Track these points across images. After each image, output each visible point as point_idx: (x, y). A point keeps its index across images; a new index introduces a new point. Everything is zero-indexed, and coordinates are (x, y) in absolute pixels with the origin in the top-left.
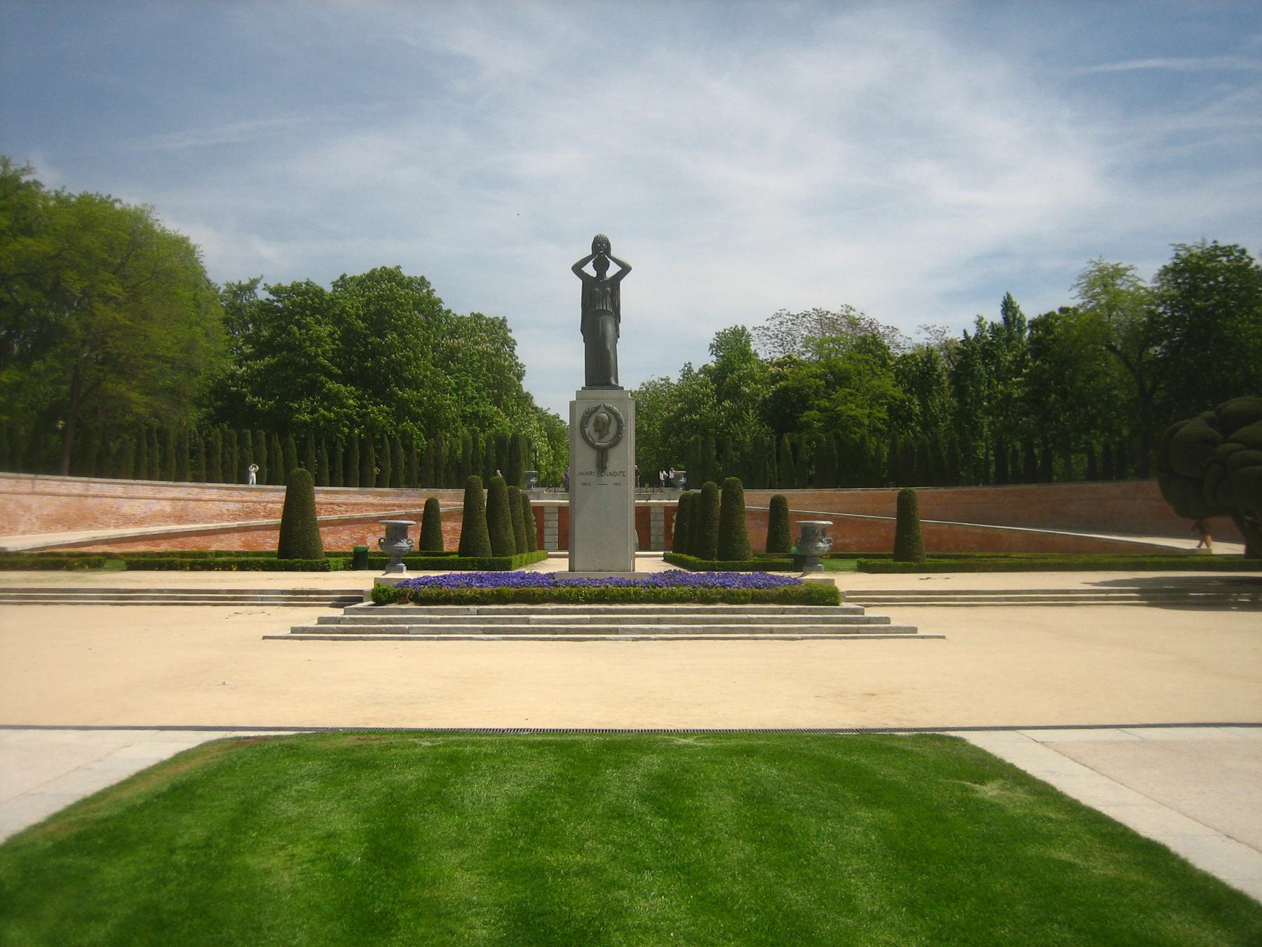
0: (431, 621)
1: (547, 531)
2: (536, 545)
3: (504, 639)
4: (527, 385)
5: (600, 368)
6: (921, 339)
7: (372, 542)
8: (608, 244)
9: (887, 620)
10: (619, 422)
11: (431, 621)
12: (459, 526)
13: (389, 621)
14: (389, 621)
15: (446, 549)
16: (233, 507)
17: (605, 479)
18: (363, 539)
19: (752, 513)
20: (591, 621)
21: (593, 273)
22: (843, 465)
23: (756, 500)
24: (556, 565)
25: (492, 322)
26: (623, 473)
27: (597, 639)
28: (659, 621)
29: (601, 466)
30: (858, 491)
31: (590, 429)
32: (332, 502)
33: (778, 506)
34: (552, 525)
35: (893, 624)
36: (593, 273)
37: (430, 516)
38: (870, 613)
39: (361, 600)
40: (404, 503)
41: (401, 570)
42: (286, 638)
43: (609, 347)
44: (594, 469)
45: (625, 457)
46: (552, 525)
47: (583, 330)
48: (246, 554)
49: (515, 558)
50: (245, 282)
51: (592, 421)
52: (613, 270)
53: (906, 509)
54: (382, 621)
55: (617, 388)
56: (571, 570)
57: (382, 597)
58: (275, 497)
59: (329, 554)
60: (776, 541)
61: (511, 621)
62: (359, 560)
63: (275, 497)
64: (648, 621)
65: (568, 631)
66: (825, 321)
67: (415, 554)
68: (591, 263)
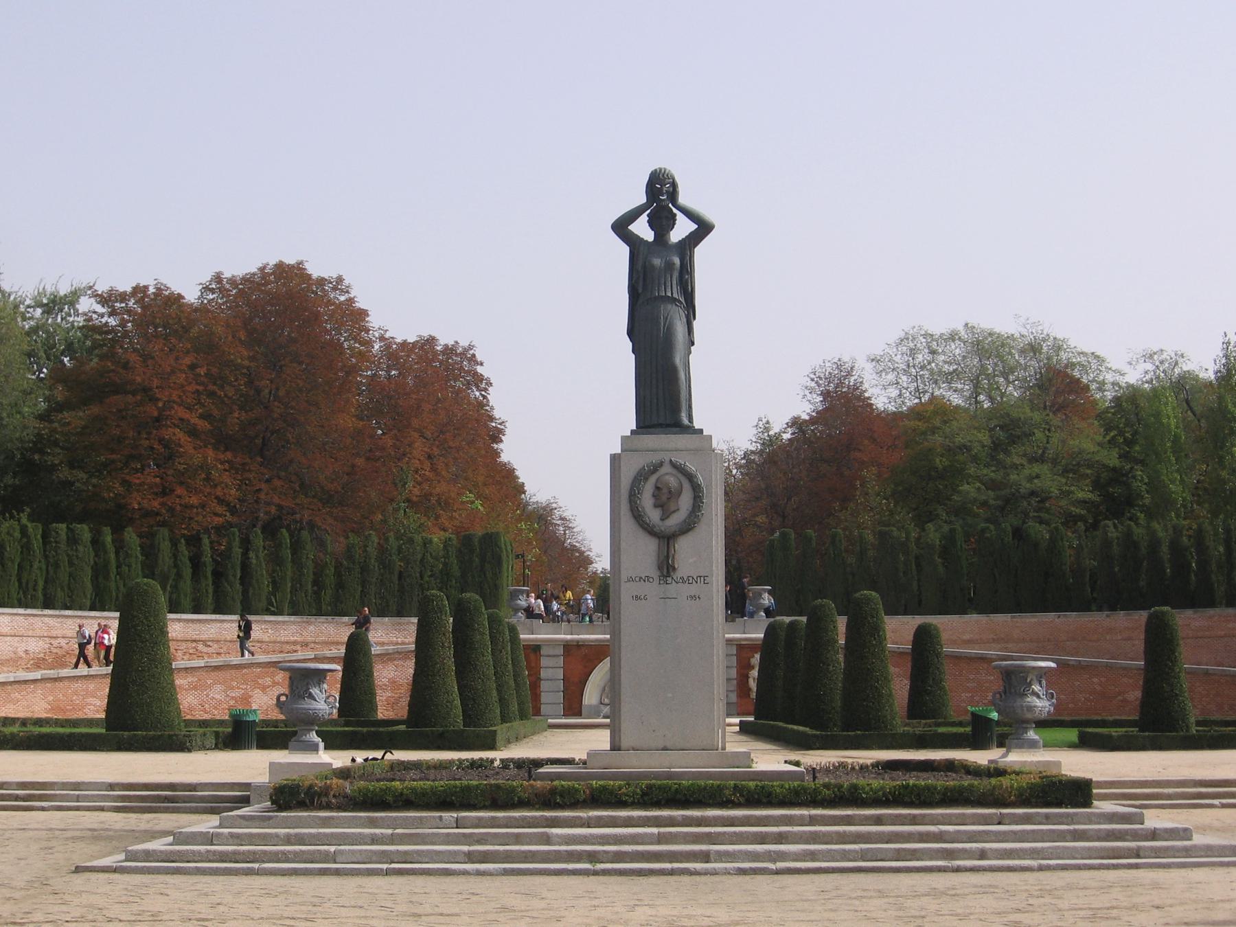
0: (374, 840)
1: (544, 686)
2: (527, 709)
3: (506, 872)
4: (510, 451)
5: (661, 395)
6: (1134, 376)
7: (263, 703)
8: (674, 185)
9: (1185, 834)
10: (696, 489)
11: (374, 840)
12: (409, 668)
13: (300, 840)
14: (300, 840)
15: (380, 716)
16: (36, 646)
17: (672, 588)
18: (246, 699)
19: (893, 652)
20: (660, 839)
21: (648, 235)
22: (1023, 578)
23: (898, 631)
24: (572, 745)
25: (449, 351)
26: (704, 579)
27: (672, 872)
28: (780, 838)
29: (666, 568)
30: (1052, 616)
31: (647, 501)
32: (197, 639)
33: (924, 640)
34: (552, 672)
35: (1198, 839)
36: (648, 235)
37: (356, 658)
38: (1155, 819)
39: (245, 801)
40: (319, 639)
41: (314, 748)
42: (115, 870)
43: (678, 361)
44: (654, 573)
45: (705, 553)
46: (552, 672)
47: (631, 333)
48: (57, 723)
49: (501, 730)
50: (64, 290)
51: (648, 488)
52: (682, 229)
53: (1160, 645)
54: (288, 840)
55: (690, 430)
56: (615, 747)
57: (289, 796)
58: (105, 625)
59: (189, 723)
60: (925, 701)
61: (518, 839)
62: (238, 733)
63: (105, 625)
64: (762, 839)
65: (619, 857)
66: (987, 348)
67: (332, 722)
68: (644, 218)
